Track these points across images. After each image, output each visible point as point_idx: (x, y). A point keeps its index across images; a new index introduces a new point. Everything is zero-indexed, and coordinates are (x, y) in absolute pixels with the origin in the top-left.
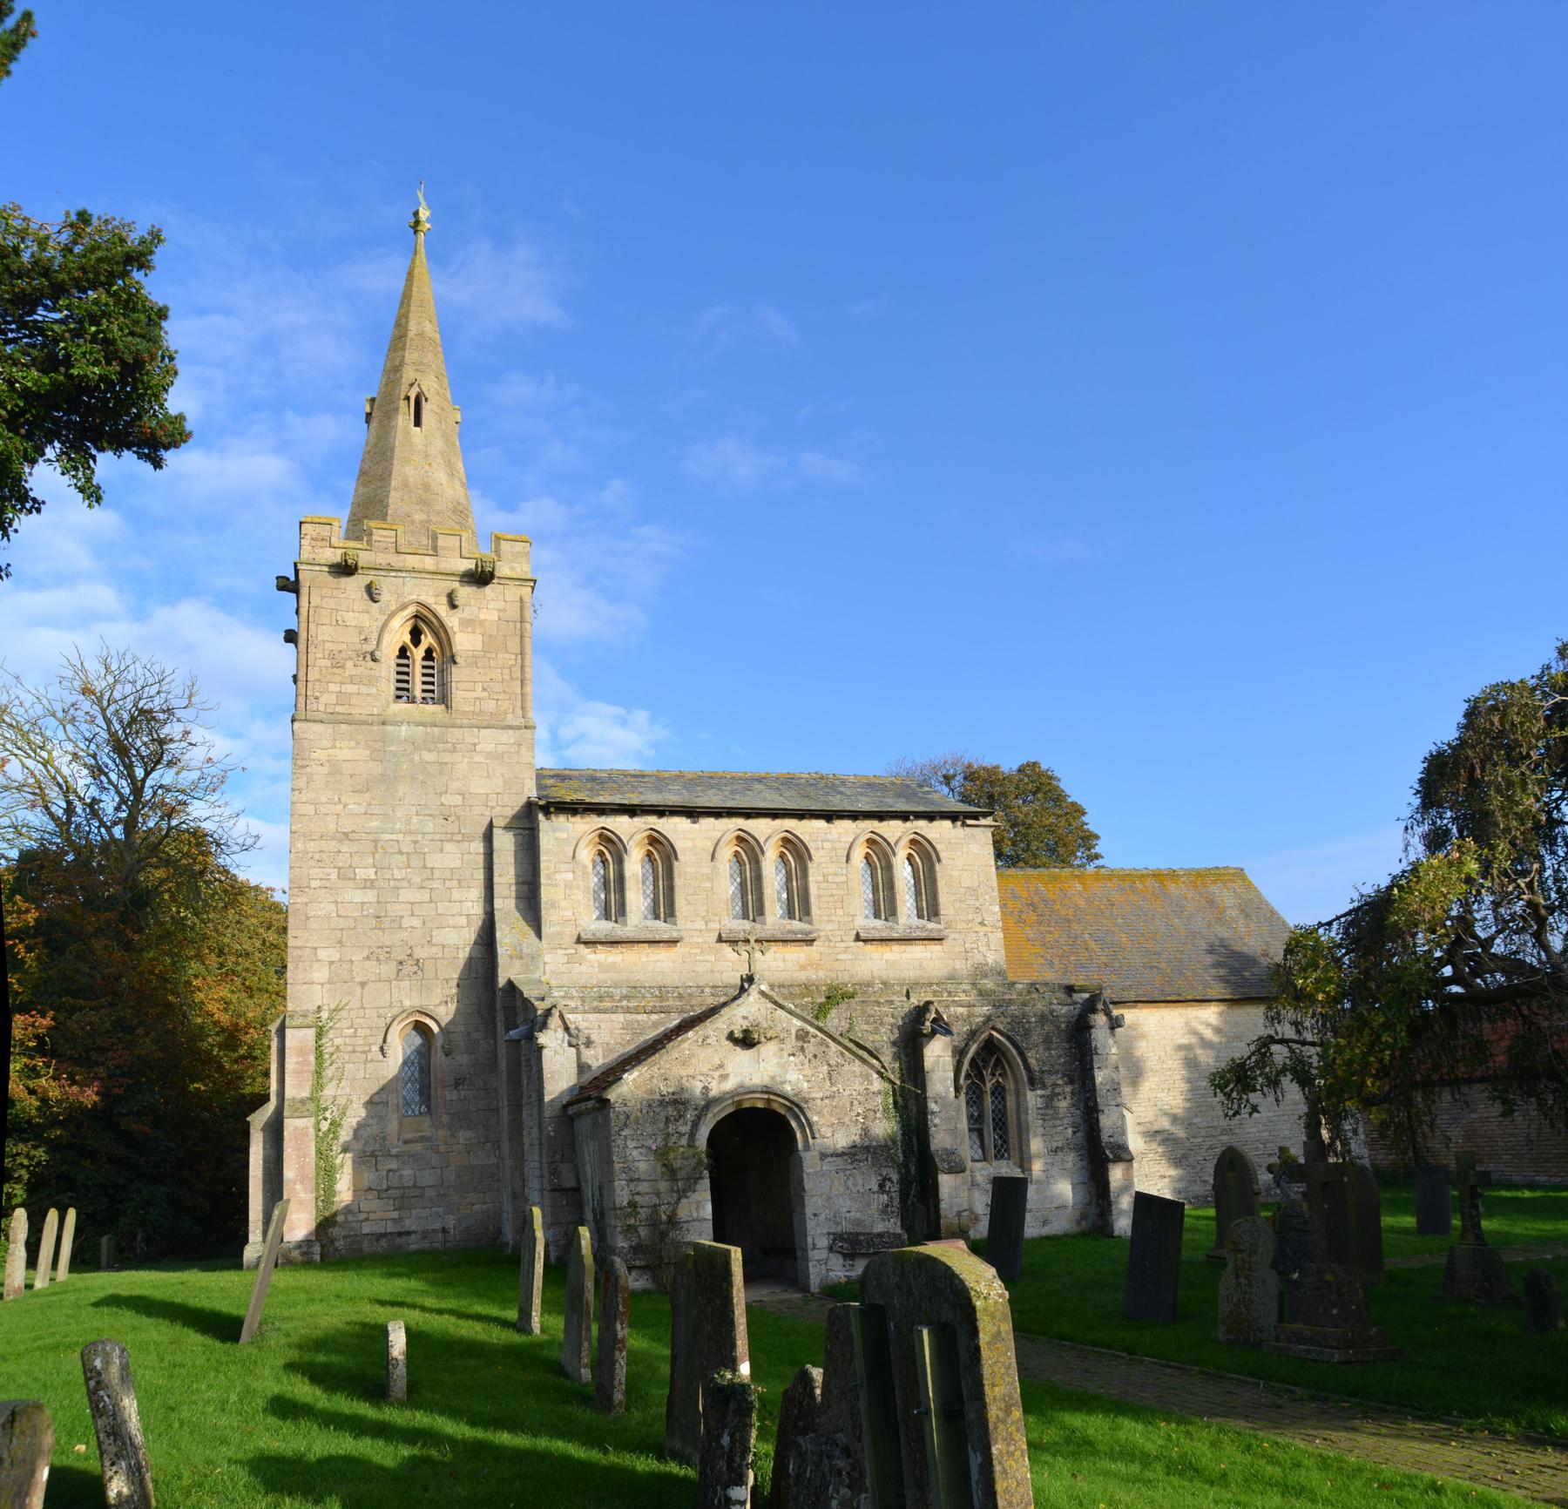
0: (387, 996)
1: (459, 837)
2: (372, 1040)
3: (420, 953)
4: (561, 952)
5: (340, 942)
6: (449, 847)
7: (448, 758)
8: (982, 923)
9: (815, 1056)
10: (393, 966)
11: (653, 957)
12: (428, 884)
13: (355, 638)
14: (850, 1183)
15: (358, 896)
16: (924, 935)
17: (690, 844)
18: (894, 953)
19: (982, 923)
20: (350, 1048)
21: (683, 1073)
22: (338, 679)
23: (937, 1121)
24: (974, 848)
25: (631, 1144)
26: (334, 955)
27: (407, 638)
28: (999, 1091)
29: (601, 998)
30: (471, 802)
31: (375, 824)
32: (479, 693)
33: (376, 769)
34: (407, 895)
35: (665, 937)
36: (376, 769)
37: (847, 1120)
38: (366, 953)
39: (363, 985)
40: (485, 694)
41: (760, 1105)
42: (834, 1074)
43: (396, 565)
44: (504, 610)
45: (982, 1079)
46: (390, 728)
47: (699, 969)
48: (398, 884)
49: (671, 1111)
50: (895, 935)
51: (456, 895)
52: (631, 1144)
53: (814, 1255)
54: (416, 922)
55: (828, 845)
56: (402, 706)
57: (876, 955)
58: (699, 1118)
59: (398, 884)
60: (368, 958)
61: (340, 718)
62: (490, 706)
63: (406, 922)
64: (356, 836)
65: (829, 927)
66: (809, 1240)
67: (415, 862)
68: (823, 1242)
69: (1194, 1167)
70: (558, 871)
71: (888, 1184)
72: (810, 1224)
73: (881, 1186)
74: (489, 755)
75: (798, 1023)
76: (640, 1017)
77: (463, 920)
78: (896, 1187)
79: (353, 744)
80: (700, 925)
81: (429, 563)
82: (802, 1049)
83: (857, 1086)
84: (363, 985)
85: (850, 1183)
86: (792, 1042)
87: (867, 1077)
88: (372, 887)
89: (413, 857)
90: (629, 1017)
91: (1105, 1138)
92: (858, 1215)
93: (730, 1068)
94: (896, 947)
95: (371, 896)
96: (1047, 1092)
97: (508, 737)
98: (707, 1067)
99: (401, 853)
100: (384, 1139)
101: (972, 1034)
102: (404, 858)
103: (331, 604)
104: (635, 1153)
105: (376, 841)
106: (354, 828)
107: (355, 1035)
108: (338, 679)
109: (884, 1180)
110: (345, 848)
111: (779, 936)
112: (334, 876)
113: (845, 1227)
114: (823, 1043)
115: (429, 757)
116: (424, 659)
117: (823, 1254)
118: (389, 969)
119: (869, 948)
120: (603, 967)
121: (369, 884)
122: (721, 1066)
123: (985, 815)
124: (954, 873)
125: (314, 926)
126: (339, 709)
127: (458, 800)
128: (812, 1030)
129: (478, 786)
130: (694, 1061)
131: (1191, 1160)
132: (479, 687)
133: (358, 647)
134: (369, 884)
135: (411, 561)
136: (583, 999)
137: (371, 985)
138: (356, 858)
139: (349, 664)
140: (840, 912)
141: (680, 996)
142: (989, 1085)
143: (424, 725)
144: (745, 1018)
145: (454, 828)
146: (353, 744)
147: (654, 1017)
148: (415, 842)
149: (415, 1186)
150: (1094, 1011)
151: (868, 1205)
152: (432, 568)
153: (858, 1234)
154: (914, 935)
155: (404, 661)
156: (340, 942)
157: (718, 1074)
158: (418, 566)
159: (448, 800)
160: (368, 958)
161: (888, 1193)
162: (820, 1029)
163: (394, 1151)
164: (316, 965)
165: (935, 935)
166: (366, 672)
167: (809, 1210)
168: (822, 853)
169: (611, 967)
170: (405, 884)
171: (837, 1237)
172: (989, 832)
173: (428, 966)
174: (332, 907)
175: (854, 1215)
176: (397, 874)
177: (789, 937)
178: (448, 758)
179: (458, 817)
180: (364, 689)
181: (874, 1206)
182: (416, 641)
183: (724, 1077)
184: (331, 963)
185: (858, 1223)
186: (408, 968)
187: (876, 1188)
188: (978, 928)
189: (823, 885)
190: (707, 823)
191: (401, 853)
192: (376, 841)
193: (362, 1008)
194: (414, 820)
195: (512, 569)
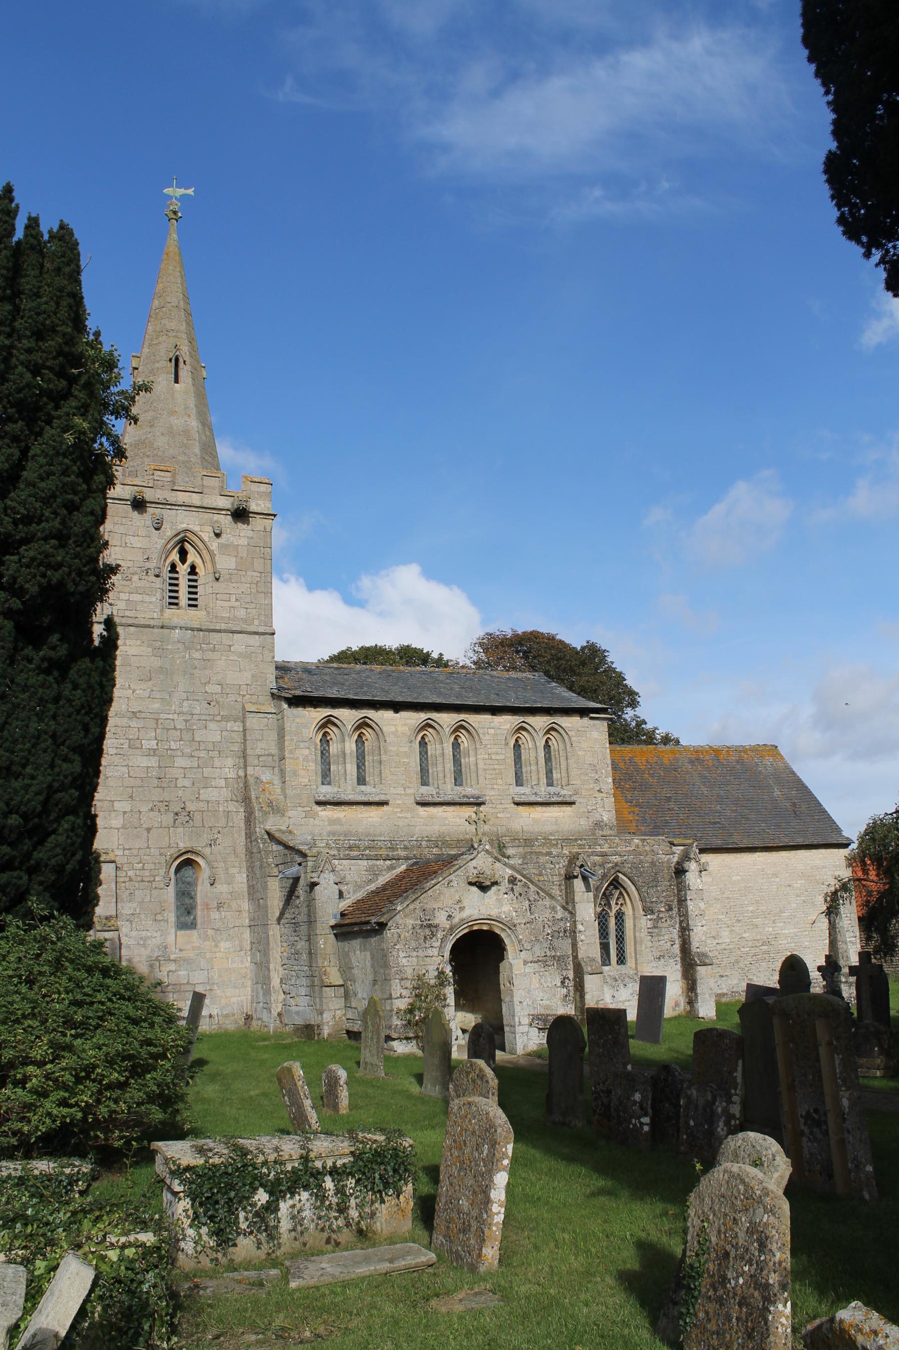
0: (167, 839)
1: (219, 718)
2: (156, 872)
3: (190, 807)
4: (299, 809)
5: (131, 797)
6: (212, 726)
7: (210, 655)
8: (599, 791)
9: (520, 894)
10: (171, 816)
11: (366, 814)
12: (196, 753)
13: (140, 558)
14: (542, 981)
15: (144, 762)
16: (560, 799)
17: (393, 729)
18: (538, 813)
19: (599, 791)
20: (139, 879)
21: (436, 906)
22: (127, 590)
23: (583, 937)
24: (595, 734)
25: (402, 954)
26: (126, 806)
27: (175, 556)
28: (620, 916)
29: (350, 848)
30: (228, 691)
31: (156, 706)
32: (233, 603)
33: (156, 662)
34: (180, 762)
35: (377, 799)
36: (156, 662)
37: (541, 938)
38: (151, 805)
39: (149, 830)
40: (238, 604)
41: (485, 928)
42: (533, 907)
43: (172, 500)
44: (252, 538)
45: (610, 907)
46: (165, 630)
47: (400, 823)
48: (173, 753)
49: (427, 932)
50: (540, 800)
51: (217, 763)
52: (402, 954)
53: (519, 1029)
54: (187, 783)
55: (492, 731)
56: (169, 612)
57: (527, 814)
58: (445, 936)
59: (173, 753)
60: (152, 809)
61: (130, 621)
62: (242, 613)
63: (180, 783)
64: (143, 715)
65: (492, 793)
66: (517, 1019)
67: (187, 736)
68: (526, 1021)
69: (743, 969)
70: (297, 747)
71: (567, 981)
72: (517, 1008)
73: (563, 983)
74: (241, 655)
75: (509, 872)
76: (378, 862)
77: (222, 783)
78: (572, 984)
79: (139, 642)
80: (400, 791)
81: (196, 499)
82: (512, 890)
83: (548, 914)
84: (149, 830)
85: (542, 981)
86: (505, 885)
87: (553, 908)
88: (155, 755)
89: (184, 732)
90: (371, 862)
91: (694, 949)
92: (548, 1002)
93: (465, 903)
94: (539, 809)
95: (153, 762)
96: (654, 917)
97: (255, 640)
98: (451, 902)
99: (175, 728)
100: (166, 947)
101: (604, 876)
102: (178, 733)
103: (122, 529)
104: (404, 960)
105: (157, 720)
106: (140, 708)
107: (143, 869)
108: (127, 590)
109: (564, 979)
110: (133, 724)
111: (457, 800)
112: (126, 746)
113: (540, 1011)
114: (525, 885)
115: (197, 655)
116: (189, 574)
117: (525, 1029)
118: (168, 818)
119: (520, 808)
120: (332, 822)
121: (153, 752)
122: (460, 901)
123: (604, 711)
124: (580, 753)
125: (112, 784)
126: (128, 613)
127: (218, 689)
128: (519, 877)
129: (232, 678)
130: (442, 897)
131: (741, 965)
132: (233, 598)
133: (142, 564)
134: (153, 752)
135: (181, 497)
136: (339, 850)
137: (154, 830)
138: (142, 731)
139: (135, 578)
140: (500, 781)
141: (406, 848)
142: (614, 911)
143: (192, 629)
144: (475, 868)
145: (214, 710)
146: (139, 642)
147: (388, 862)
148: (186, 721)
149: (188, 983)
150: (689, 859)
151: (554, 995)
152: (198, 504)
153: (548, 1015)
154: (553, 800)
155: (176, 575)
156: (131, 797)
157: (457, 907)
158: (188, 501)
159: (209, 688)
160: (152, 809)
161: (567, 987)
162: (524, 876)
163: (172, 957)
164: (113, 814)
165: (568, 799)
166: (148, 585)
167: (516, 1000)
168: (487, 737)
169: (337, 821)
170: (179, 753)
171: (535, 1018)
172: (605, 723)
173: (197, 817)
174: (125, 769)
175: (545, 1002)
176: (173, 745)
177: (465, 800)
178: (210, 655)
179: (218, 702)
180: (147, 598)
181: (558, 996)
182: (183, 559)
183: (462, 909)
184: (125, 813)
185: (547, 1007)
186: (182, 818)
187: (559, 984)
188: (598, 795)
189: (488, 762)
190: (404, 714)
191: (175, 728)
192: (157, 720)
193: (148, 847)
194: (185, 704)
195: (257, 505)
